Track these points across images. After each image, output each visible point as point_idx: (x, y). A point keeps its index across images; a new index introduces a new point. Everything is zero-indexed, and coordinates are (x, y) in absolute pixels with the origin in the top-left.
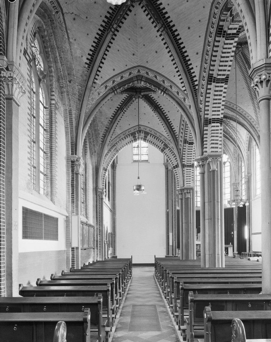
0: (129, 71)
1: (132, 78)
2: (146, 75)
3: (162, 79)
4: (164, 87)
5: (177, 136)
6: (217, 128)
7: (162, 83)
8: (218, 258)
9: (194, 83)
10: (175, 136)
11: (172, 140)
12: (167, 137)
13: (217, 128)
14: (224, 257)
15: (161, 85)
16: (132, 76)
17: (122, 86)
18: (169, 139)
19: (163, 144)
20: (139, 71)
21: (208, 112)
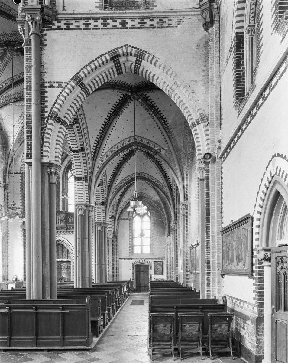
0: (129, 139)
1: (130, 144)
2: (141, 142)
3: (147, 142)
4: (155, 150)
5: (171, 185)
6: (97, 200)
7: (153, 147)
8: (98, 256)
9: (44, 103)
10: (170, 185)
11: (166, 185)
12: (163, 183)
13: (97, 200)
14: (56, 265)
15: (152, 148)
16: (130, 142)
17: (126, 149)
18: (164, 184)
19: (85, 174)
20: (136, 139)
21: (84, 165)
